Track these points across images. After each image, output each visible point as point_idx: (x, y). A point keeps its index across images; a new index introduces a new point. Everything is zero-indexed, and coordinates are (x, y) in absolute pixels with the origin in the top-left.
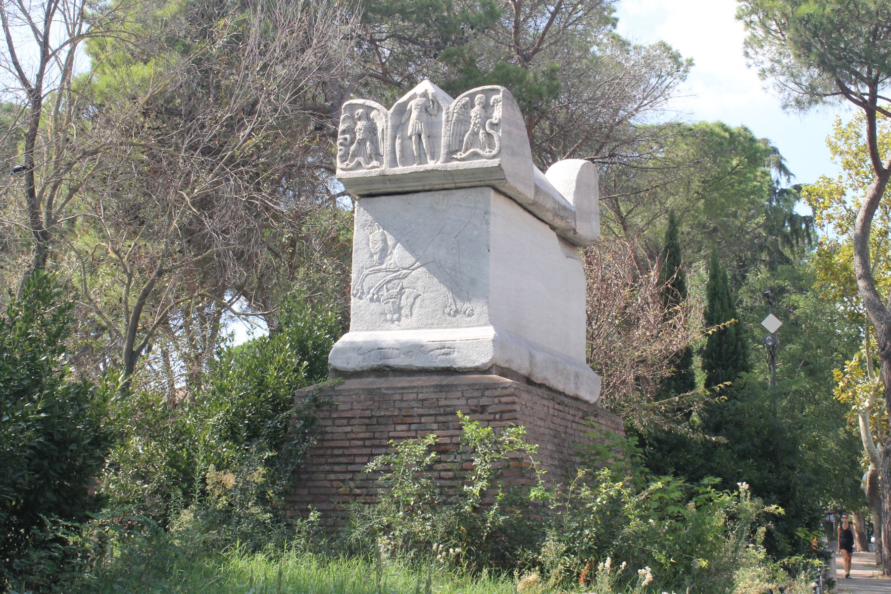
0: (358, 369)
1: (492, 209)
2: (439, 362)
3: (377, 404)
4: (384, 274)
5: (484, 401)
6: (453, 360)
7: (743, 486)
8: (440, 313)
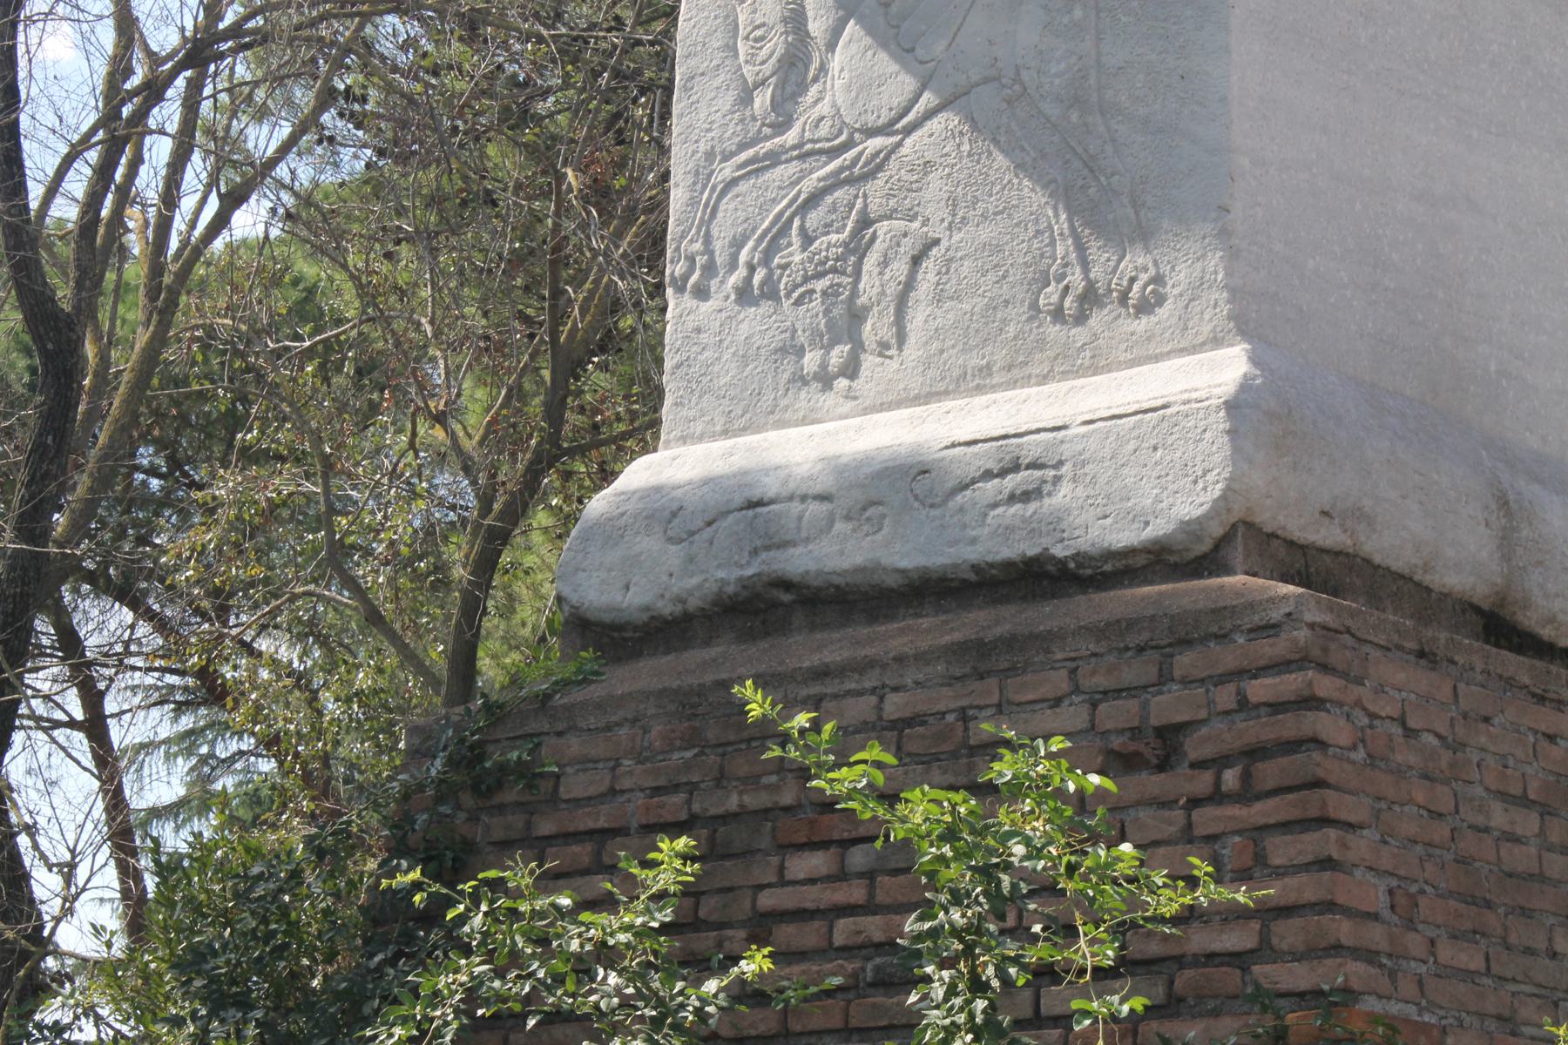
0: (667, 609)
2: (994, 536)
3: (712, 758)
4: (793, 168)
5: (1167, 707)
6: (1055, 523)
8: (1019, 311)
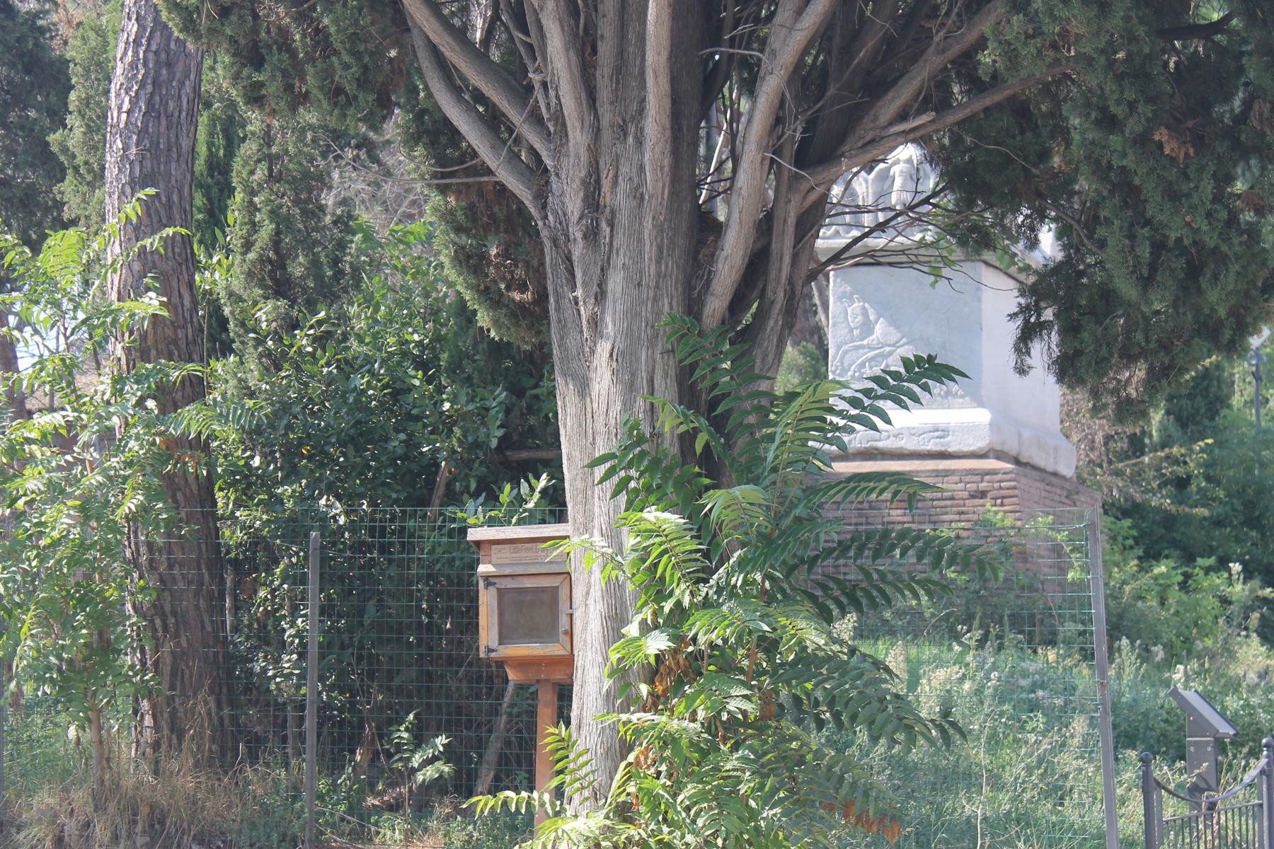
5: (983, 486)
7: (1236, 567)
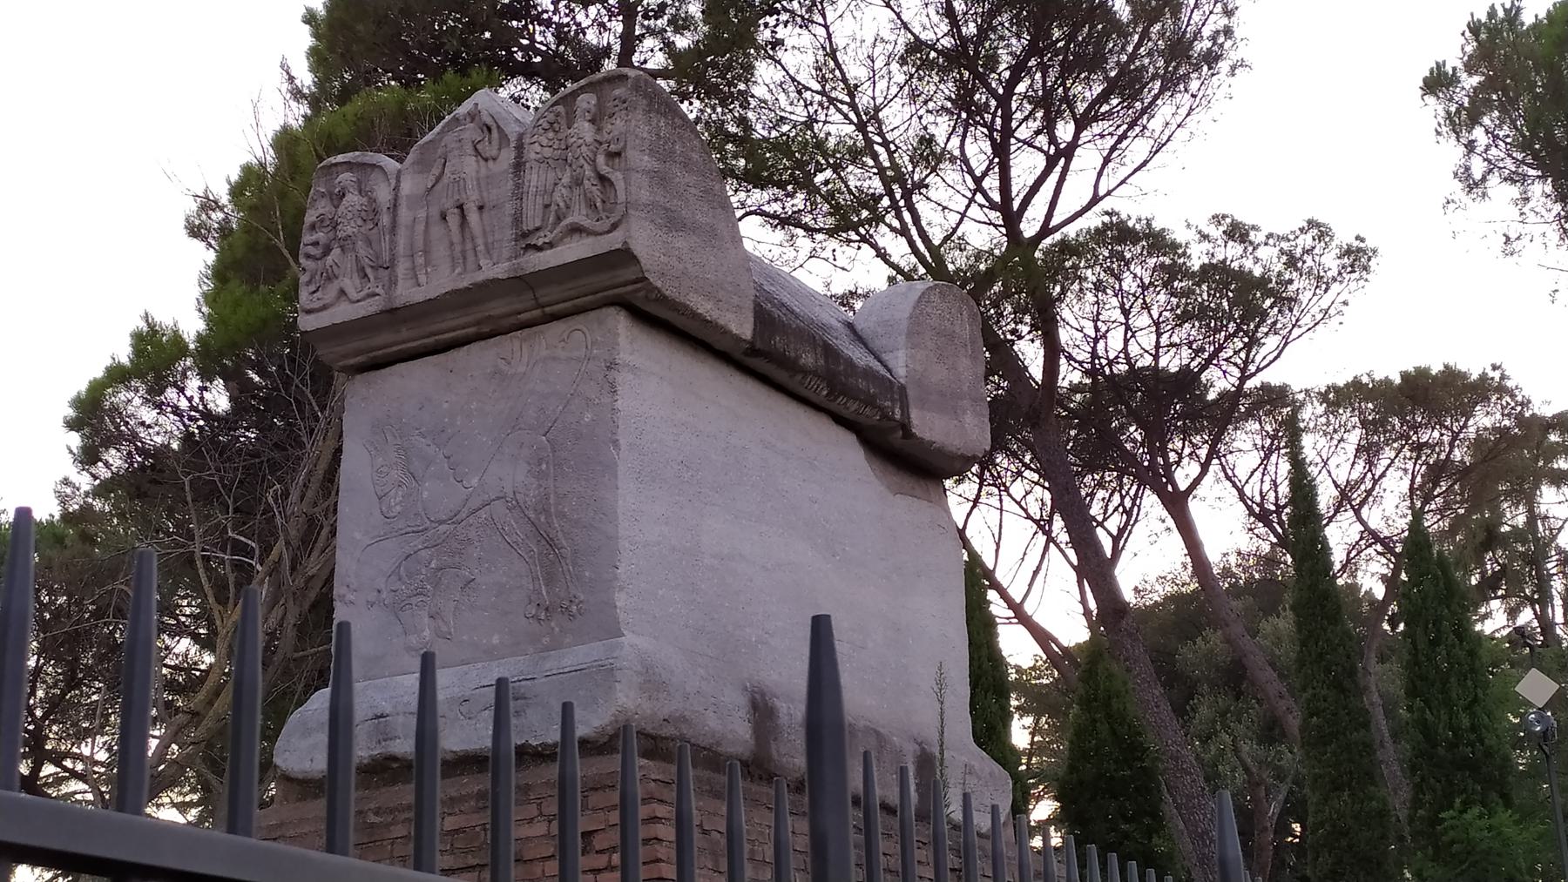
1: (624, 356)
